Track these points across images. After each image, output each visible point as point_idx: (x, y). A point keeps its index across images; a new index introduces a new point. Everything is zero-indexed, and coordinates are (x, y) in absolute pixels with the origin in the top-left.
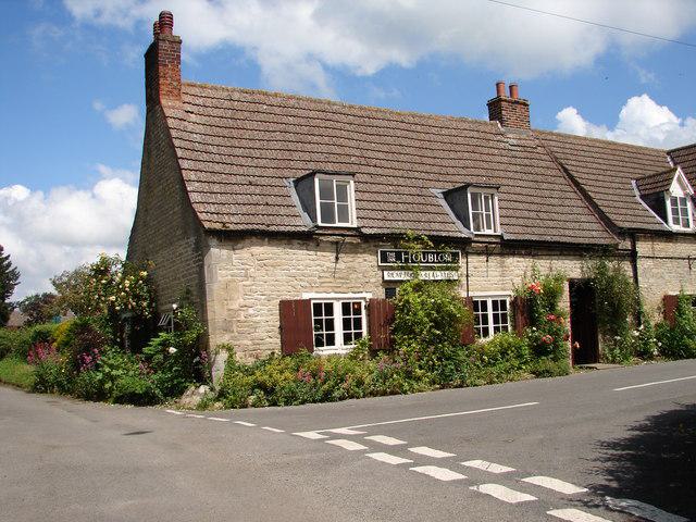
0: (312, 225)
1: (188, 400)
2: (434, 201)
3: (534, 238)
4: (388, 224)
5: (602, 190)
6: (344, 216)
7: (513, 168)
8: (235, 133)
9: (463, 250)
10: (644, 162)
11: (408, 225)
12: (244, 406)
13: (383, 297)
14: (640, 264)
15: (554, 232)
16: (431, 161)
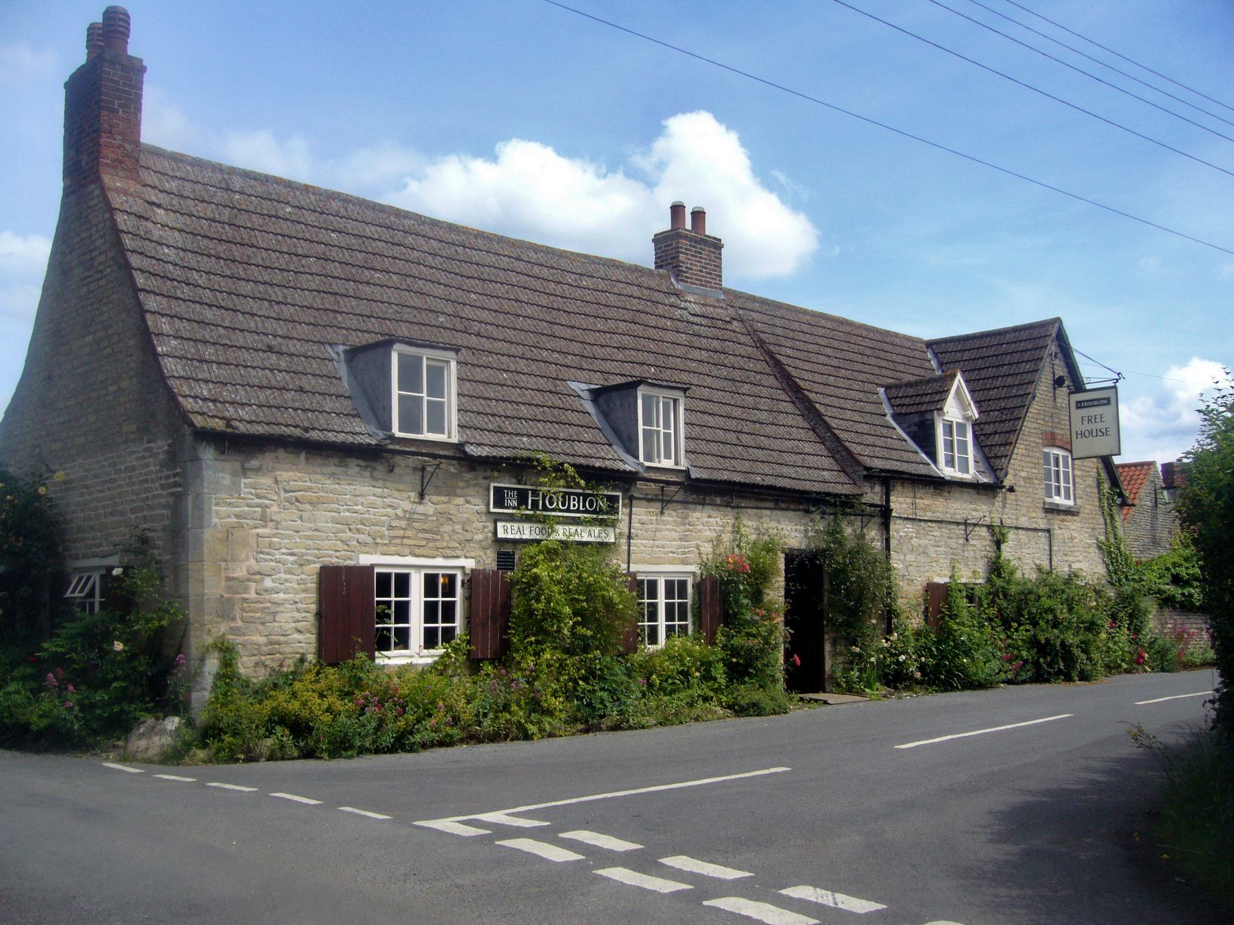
0: (381, 434)
1: (143, 743)
2: (577, 403)
3: (737, 478)
4: (505, 440)
5: (835, 402)
6: (437, 424)
7: (696, 354)
8: (237, 252)
9: (626, 491)
10: (894, 357)
11: (538, 443)
12: (251, 758)
13: (495, 568)
14: (898, 530)
15: (766, 469)
16: (567, 333)
